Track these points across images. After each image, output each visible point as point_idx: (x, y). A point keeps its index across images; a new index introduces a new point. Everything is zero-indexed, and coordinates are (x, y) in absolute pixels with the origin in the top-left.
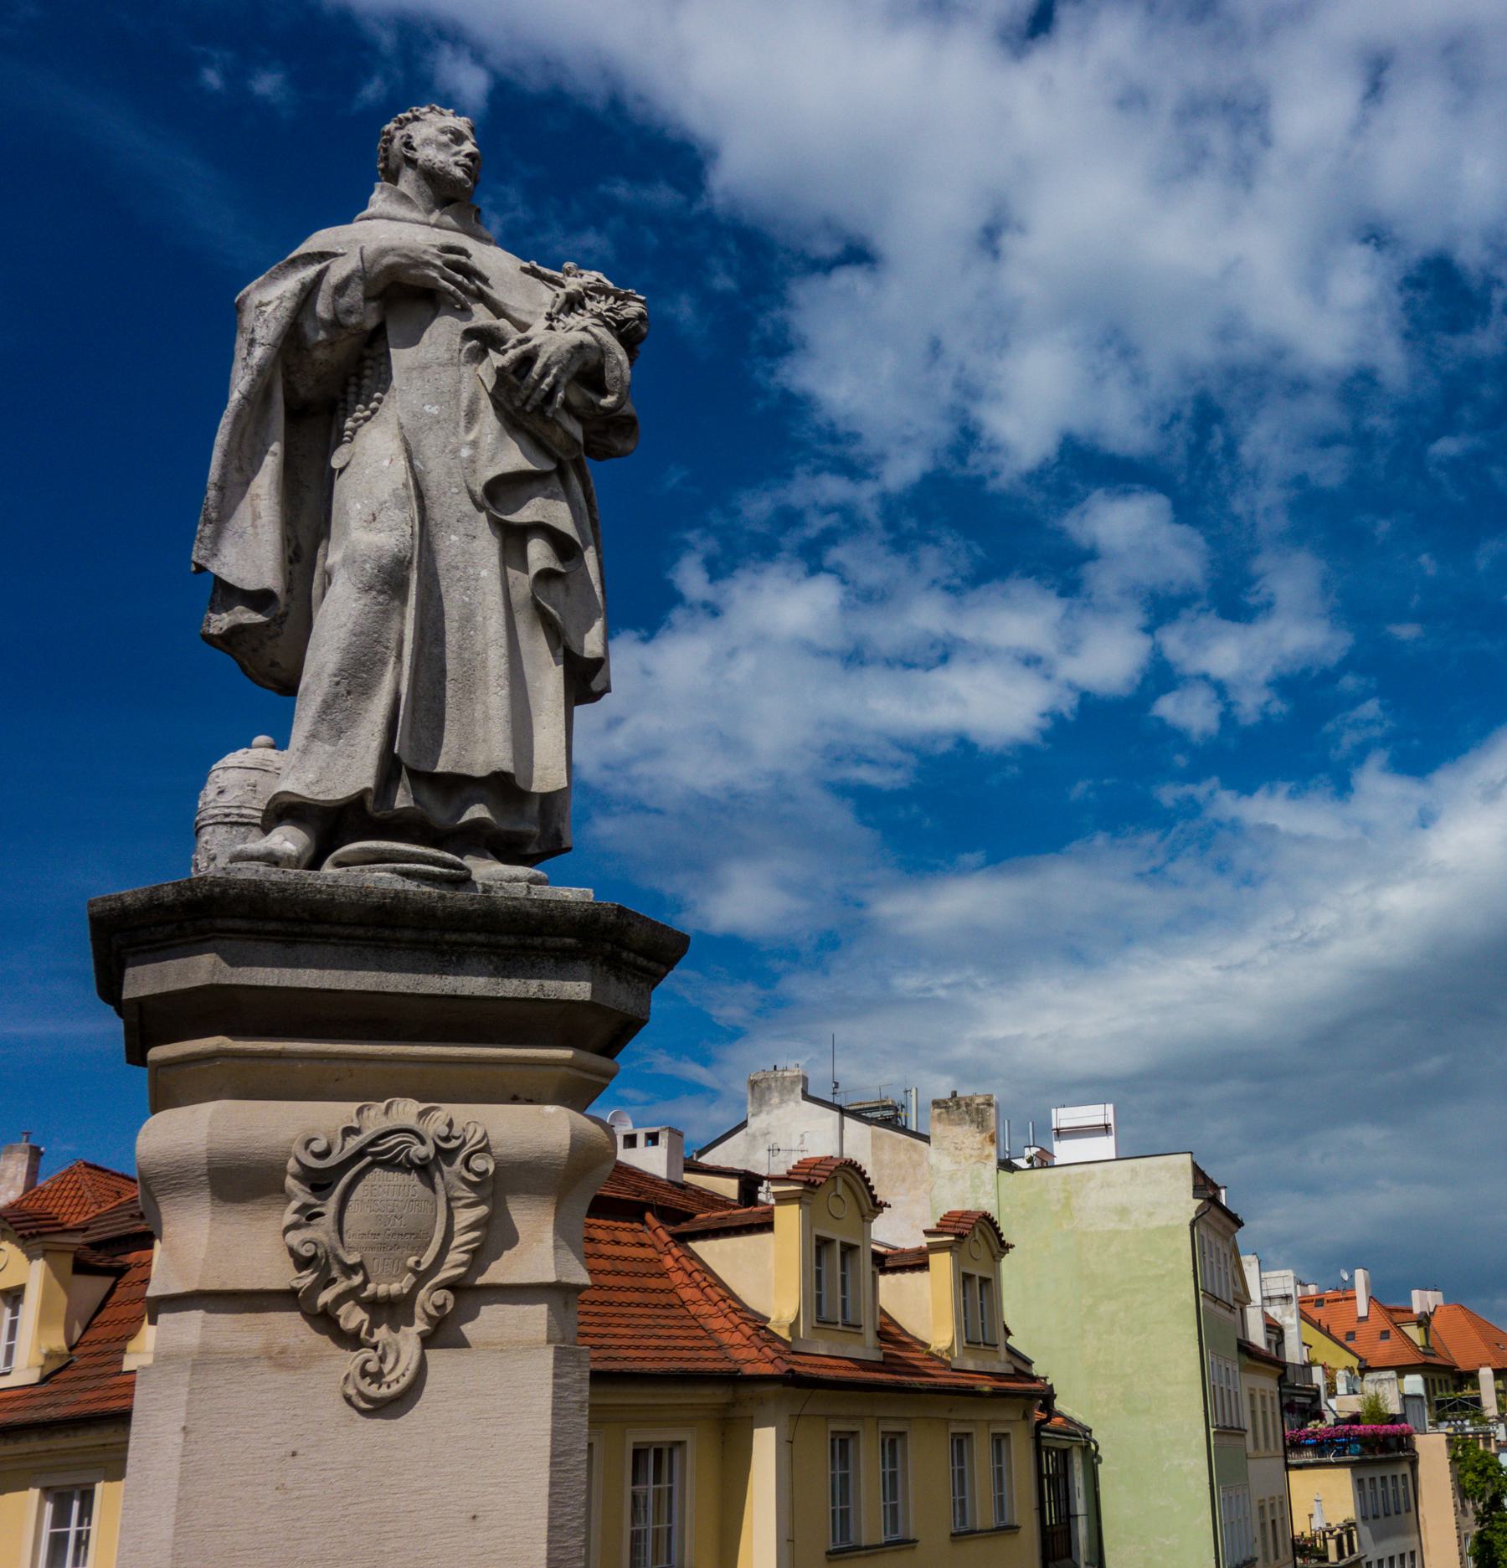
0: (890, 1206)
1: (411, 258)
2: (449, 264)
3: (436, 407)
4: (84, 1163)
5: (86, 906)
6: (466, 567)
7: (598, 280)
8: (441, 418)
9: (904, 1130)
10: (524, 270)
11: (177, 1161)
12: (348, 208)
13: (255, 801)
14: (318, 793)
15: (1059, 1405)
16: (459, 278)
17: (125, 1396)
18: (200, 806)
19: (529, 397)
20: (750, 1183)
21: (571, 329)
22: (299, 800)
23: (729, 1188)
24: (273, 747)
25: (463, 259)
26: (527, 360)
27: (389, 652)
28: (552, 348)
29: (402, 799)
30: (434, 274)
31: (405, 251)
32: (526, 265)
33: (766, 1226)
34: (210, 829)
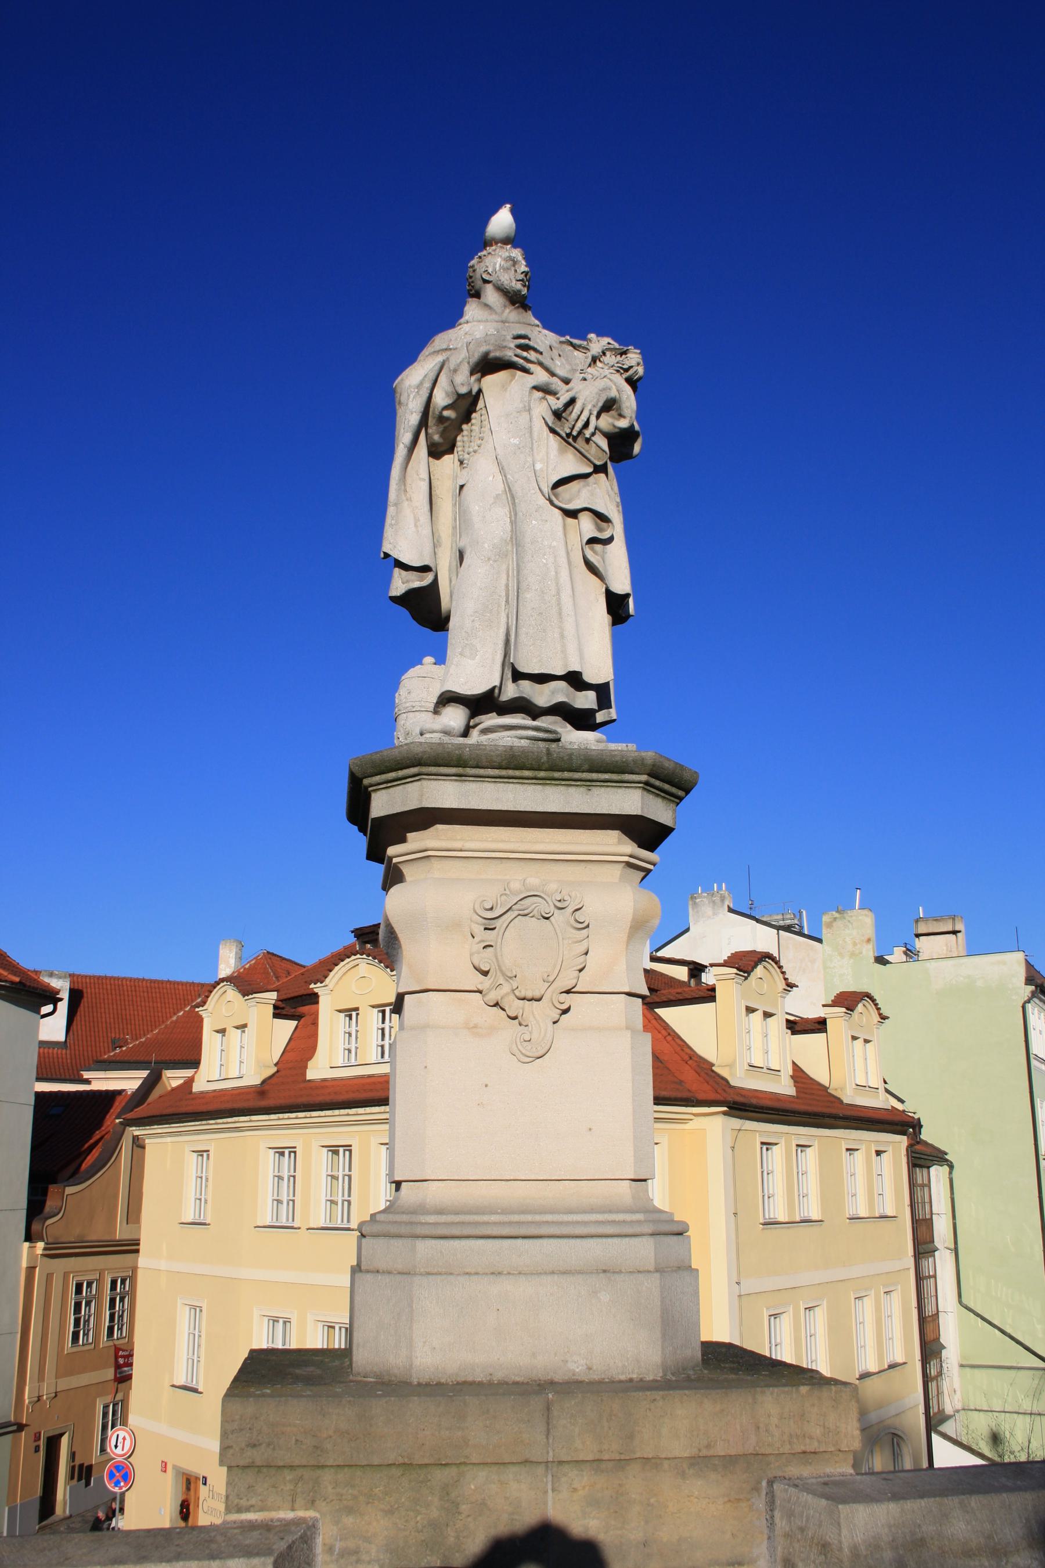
0: (797, 986)
2: (519, 347)
4: (268, 952)
6: (543, 540)
7: (609, 343)
8: (521, 446)
9: (801, 934)
10: (561, 342)
12: (452, 318)
15: (924, 1136)
18: (397, 702)
19: (574, 426)
20: (696, 969)
21: (597, 378)
22: (456, 695)
23: (681, 973)
24: (435, 664)
25: (526, 341)
26: (572, 401)
28: (587, 393)
29: (511, 691)
32: (563, 339)
33: (709, 995)
34: (405, 715)
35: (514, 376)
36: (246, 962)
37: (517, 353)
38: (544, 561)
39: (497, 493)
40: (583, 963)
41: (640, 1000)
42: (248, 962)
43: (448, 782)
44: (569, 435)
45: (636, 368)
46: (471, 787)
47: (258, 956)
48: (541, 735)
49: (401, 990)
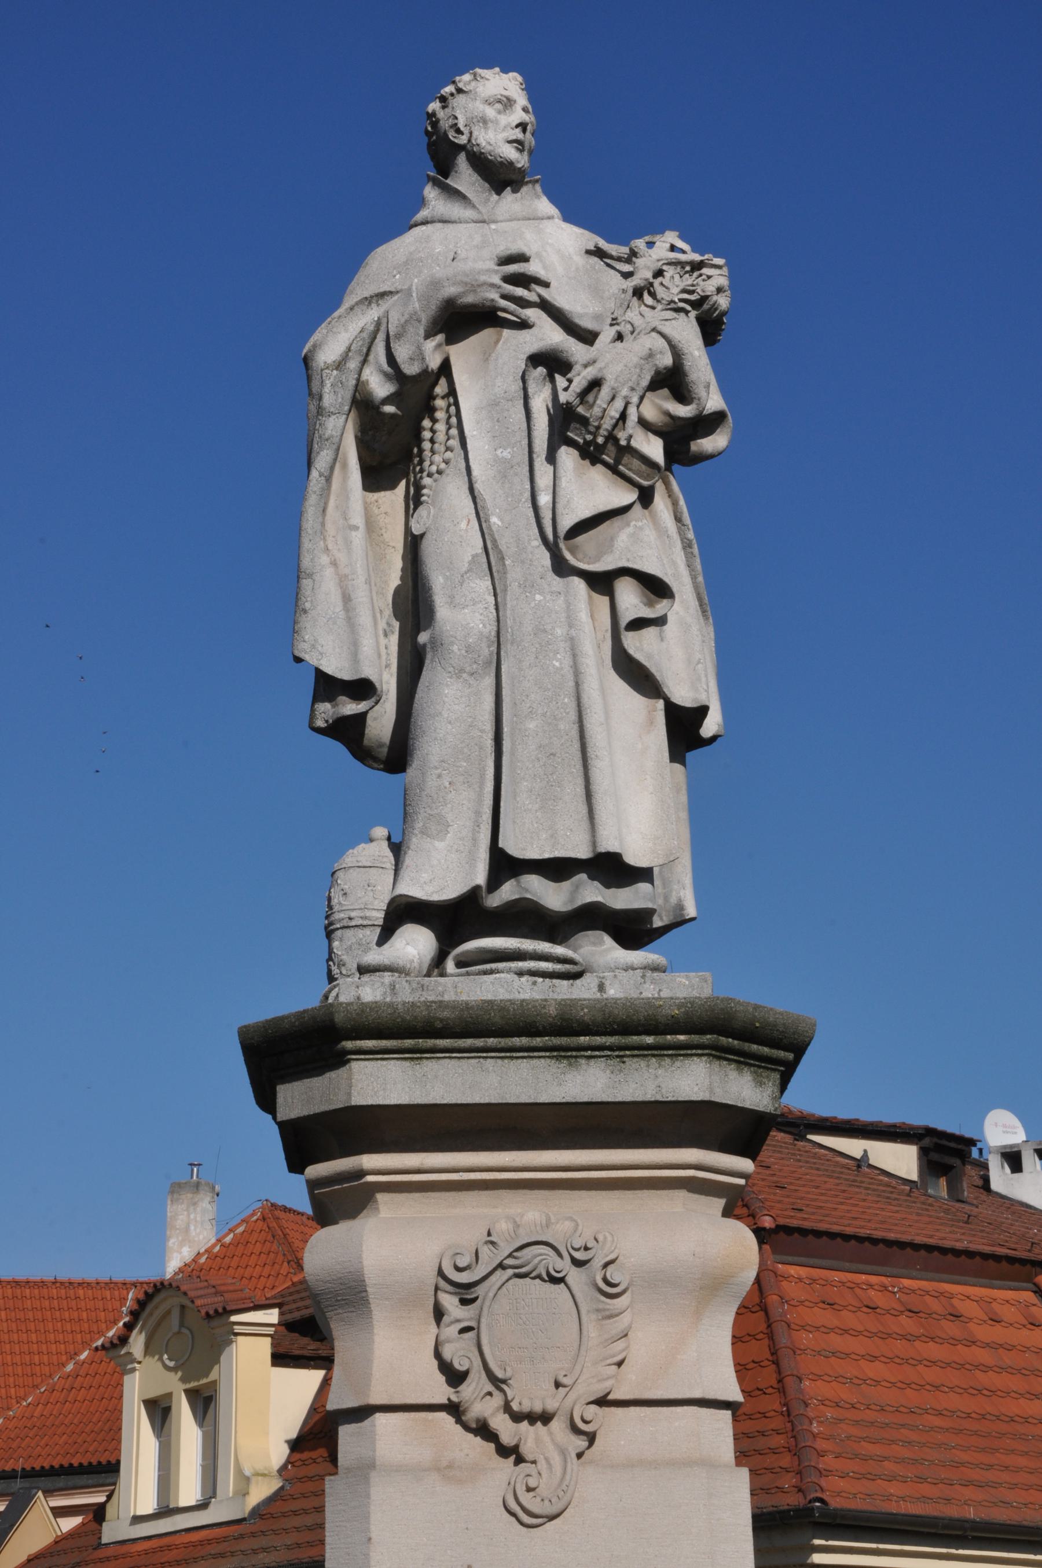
1: (466, 284)
2: (510, 279)
3: (509, 450)
4: (273, 1205)
5: (492, 265)
6: (553, 628)
7: (673, 248)
11: (340, 1278)
13: (376, 902)
14: (432, 893)
16: (520, 292)
17: (310, 1544)
22: (416, 900)
26: (595, 384)
27: (484, 735)
28: (619, 367)
29: (508, 892)
30: (494, 295)
31: (459, 278)
36: (226, 1230)
37: (506, 292)
38: (557, 664)
39: (474, 553)
40: (623, 1350)
41: (728, 1414)
42: (231, 1230)
43: (392, 1062)
45: (715, 298)
46: (431, 1067)
47: (253, 1215)
48: (559, 967)
49: (335, 1402)
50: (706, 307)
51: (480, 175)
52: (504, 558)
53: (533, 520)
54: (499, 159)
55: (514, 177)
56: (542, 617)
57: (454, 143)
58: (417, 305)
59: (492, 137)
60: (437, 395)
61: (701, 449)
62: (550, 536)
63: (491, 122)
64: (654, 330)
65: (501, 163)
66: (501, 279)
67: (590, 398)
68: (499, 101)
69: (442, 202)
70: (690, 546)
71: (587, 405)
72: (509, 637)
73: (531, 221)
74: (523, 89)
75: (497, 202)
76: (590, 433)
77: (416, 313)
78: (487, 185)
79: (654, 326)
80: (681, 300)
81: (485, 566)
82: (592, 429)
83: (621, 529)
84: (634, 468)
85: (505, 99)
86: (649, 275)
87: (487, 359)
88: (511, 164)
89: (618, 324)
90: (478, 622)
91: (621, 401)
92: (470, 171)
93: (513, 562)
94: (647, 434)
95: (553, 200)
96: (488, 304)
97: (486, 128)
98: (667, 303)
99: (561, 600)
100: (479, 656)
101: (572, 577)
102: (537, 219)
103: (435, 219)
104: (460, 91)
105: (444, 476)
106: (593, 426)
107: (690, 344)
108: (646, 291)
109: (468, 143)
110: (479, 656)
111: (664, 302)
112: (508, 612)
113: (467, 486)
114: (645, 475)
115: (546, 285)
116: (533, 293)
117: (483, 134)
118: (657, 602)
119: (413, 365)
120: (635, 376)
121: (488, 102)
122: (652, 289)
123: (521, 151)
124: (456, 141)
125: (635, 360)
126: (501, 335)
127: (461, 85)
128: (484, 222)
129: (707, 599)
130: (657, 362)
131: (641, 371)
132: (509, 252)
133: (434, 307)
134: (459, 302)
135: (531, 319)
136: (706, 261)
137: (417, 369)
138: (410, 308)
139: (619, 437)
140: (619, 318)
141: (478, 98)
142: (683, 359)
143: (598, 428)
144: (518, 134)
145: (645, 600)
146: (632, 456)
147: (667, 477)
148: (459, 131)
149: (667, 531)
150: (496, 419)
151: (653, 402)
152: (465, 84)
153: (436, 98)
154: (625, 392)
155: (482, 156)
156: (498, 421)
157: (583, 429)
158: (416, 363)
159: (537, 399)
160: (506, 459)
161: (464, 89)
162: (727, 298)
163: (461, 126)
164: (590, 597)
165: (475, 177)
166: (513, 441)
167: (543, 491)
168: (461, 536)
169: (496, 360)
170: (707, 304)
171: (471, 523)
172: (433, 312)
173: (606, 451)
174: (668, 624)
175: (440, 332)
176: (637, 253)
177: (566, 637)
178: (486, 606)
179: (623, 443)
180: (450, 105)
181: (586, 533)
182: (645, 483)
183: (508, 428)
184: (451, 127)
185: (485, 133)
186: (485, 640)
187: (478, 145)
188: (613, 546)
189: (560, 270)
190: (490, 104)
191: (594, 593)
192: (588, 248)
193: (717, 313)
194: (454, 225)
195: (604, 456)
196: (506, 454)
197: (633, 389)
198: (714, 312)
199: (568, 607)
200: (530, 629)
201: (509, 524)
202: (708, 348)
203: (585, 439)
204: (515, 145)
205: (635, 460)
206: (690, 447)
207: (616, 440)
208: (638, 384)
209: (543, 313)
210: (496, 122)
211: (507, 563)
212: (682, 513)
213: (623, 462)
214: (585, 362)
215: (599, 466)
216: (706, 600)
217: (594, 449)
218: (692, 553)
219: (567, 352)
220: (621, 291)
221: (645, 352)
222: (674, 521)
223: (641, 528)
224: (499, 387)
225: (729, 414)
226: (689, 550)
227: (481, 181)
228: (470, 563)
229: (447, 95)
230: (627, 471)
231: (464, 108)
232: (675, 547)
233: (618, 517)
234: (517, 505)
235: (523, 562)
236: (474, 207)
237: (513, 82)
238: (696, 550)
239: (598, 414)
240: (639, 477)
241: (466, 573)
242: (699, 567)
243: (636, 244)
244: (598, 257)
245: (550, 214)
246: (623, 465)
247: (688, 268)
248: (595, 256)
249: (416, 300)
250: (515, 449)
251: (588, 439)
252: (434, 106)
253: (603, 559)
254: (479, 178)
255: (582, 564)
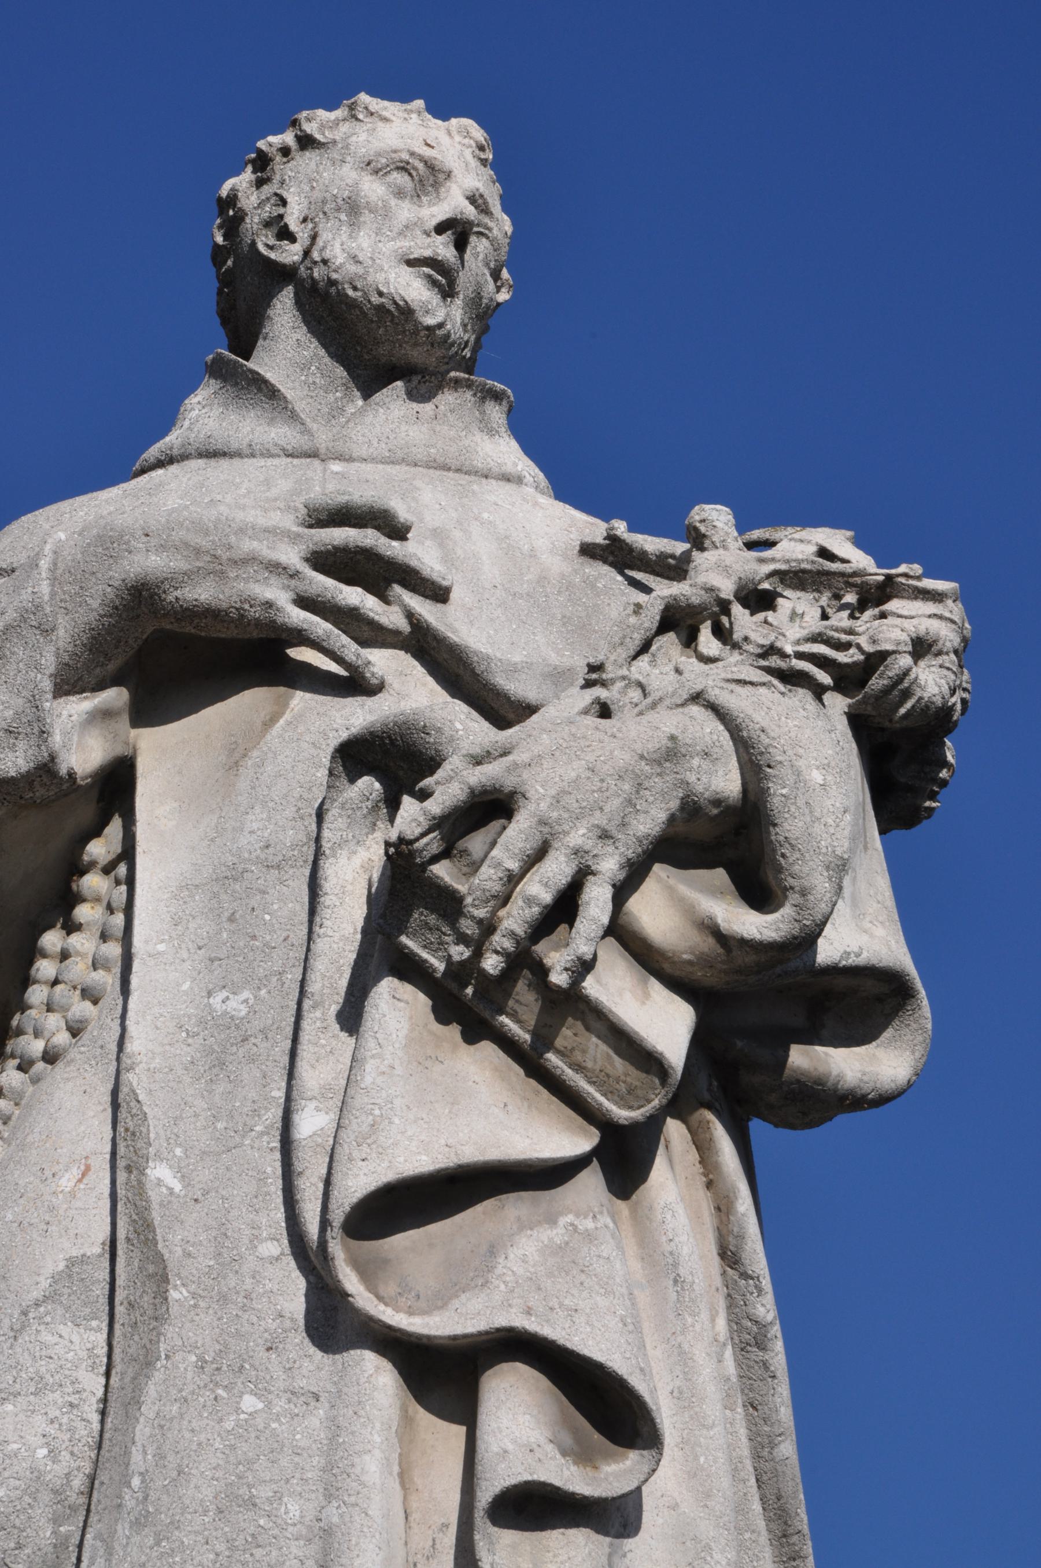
1: (198, 551)
3: (246, 994)
5: (289, 522)
6: (278, 1496)
7: (824, 553)
16: (353, 596)
28: (573, 770)
35: (282, 706)
37: (312, 591)
39: (75, 1252)
44: (460, 972)
50: (876, 683)
51: (324, 345)
52: (165, 1279)
53: (276, 1186)
54: (375, 299)
55: (416, 355)
56: (250, 1462)
57: (268, 261)
58: (45, 588)
59: (365, 245)
60: (93, 864)
61: (821, 1069)
62: (312, 1229)
63: (370, 211)
64: (697, 698)
65: (381, 309)
66: (307, 560)
67: (475, 843)
68: (404, 168)
69: (217, 411)
70: (761, 1343)
71: (465, 861)
72: (129, 1502)
73: (451, 474)
74: (484, 162)
75: (361, 412)
76: (462, 939)
77: (38, 607)
78: (340, 372)
79: (698, 687)
80: (800, 656)
81: (101, 1291)
82: (468, 927)
83: (523, 1226)
84: (589, 1065)
85: (421, 166)
86: (727, 588)
87: (236, 763)
88: (406, 312)
89: (604, 684)
90: (35, 1441)
91: (562, 858)
92: (302, 333)
93: (194, 1295)
94: (645, 982)
95: (530, 449)
96: (255, 613)
97: (354, 225)
98: (759, 651)
99: (317, 1418)
100: (19, 1547)
101: (358, 1351)
102: (468, 473)
103: (191, 450)
104: (306, 142)
105: (60, 1065)
106: (473, 918)
107: (801, 751)
108: (709, 623)
109: (302, 262)
110: (19, 1547)
111: (750, 648)
112: (142, 1431)
113: (110, 1086)
114: (622, 1087)
115: (439, 594)
116: (395, 609)
117: (344, 237)
118: (609, 1457)
119: (13, 748)
120: (616, 802)
121: (373, 167)
122: (725, 620)
123: (448, 292)
124: (273, 255)
125: (623, 758)
126: (286, 705)
127: (310, 128)
128: (313, 454)
129: (804, 1517)
130: (692, 778)
131: (638, 792)
132: (342, 499)
133: (95, 604)
134: (170, 598)
135: (375, 670)
136: (903, 580)
137: (21, 761)
138: (26, 595)
139: (548, 961)
140: (609, 667)
141: (348, 159)
142: (767, 777)
143: (488, 928)
144: (443, 248)
145: (568, 1440)
146: (588, 1029)
147: (707, 1126)
148: (286, 234)
149: (676, 1265)
150: (227, 914)
151: (671, 890)
152: (322, 127)
153: (246, 164)
154: (579, 836)
155: (333, 290)
156: (231, 919)
157: (446, 929)
158: (21, 745)
159: (343, 860)
160: (232, 1018)
161: (319, 137)
162: (945, 672)
163: (293, 222)
164: (407, 1421)
165: (313, 348)
166: (261, 972)
167: (313, 1098)
168: (52, 1209)
169: (261, 764)
170: (881, 677)
171: (91, 1176)
172: (93, 616)
173: (511, 1003)
174: (641, 1534)
175: (116, 681)
176: (704, 536)
177: (310, 1528)
178: (74, 1399)
179: (559, 978)
180: (277, 178)
181: (419, 1227)
182: (622, 1114)
183: (254, 937)
184: (267, 224)
185: (350, 236)
186: (46, 1497)
187: (325, 262)
188: (490, 1269)
189: (491, 572)
190: (376, 172)
191: (421, 1411)
192: (589, 539)
193: (909, 705)
194: (236, 462)
195: (504, 1019)
196: (237, 1005)
197: (605, 835)
198: (901, 703)
199: (332, 1439)
200: (208, 1493)
201: (206, 1193)
202: (897, 834)
203: (449, 959)
204: (427, 270)
205: (594, 1039)
206: (787, 1056)
207: (541, 971)
208: (624, 825)
209: (416, 663)
210: (385, 213)
211: (173, 1295)
212: (741, 1237)
213: (559, 1042)
214: (477, 750)
215: (488, 1049)
216: (802, 1520)
217: (474, 993)
218: (765, 1365)
219: (439, 730)
220: (632, 607)
221: (657, 742)
222: (716, 1260)
223: (589, 1237)
224: (252, 832)
225: (923, 993)
226: (757, 1354)
227: (327, 360)
228: (55, 1279)
229: (272, 152)
230: (569, 1072)
231: (311, 180)
232: (693, 1315)
233: (523, 1194)
234: (238, 1139)
235: (224, 1299)
236: (293, 416)
237: (458, 138)
238: (778, 1355)
239: (489, 885)
240: (604, 1095)
241: (37, 1305)
242: (785, 1414)
243: (704, 515)
244: (612, 565)
245: (509, 468)
246: (558, 1052)
247: (850, 598)
248: (605, 561)
249: (44, 575)
250: (263, 992)
251: (456, 958)
252: (242, 181)
253: (455, 1303)
254: (322, 352)
255: (389, 1311)
